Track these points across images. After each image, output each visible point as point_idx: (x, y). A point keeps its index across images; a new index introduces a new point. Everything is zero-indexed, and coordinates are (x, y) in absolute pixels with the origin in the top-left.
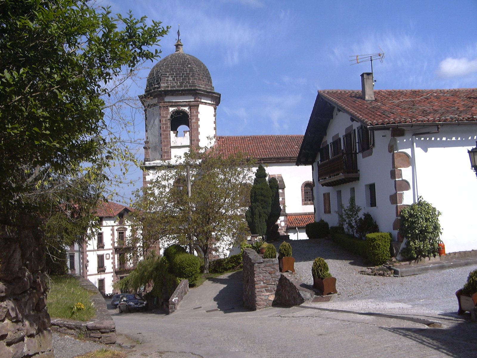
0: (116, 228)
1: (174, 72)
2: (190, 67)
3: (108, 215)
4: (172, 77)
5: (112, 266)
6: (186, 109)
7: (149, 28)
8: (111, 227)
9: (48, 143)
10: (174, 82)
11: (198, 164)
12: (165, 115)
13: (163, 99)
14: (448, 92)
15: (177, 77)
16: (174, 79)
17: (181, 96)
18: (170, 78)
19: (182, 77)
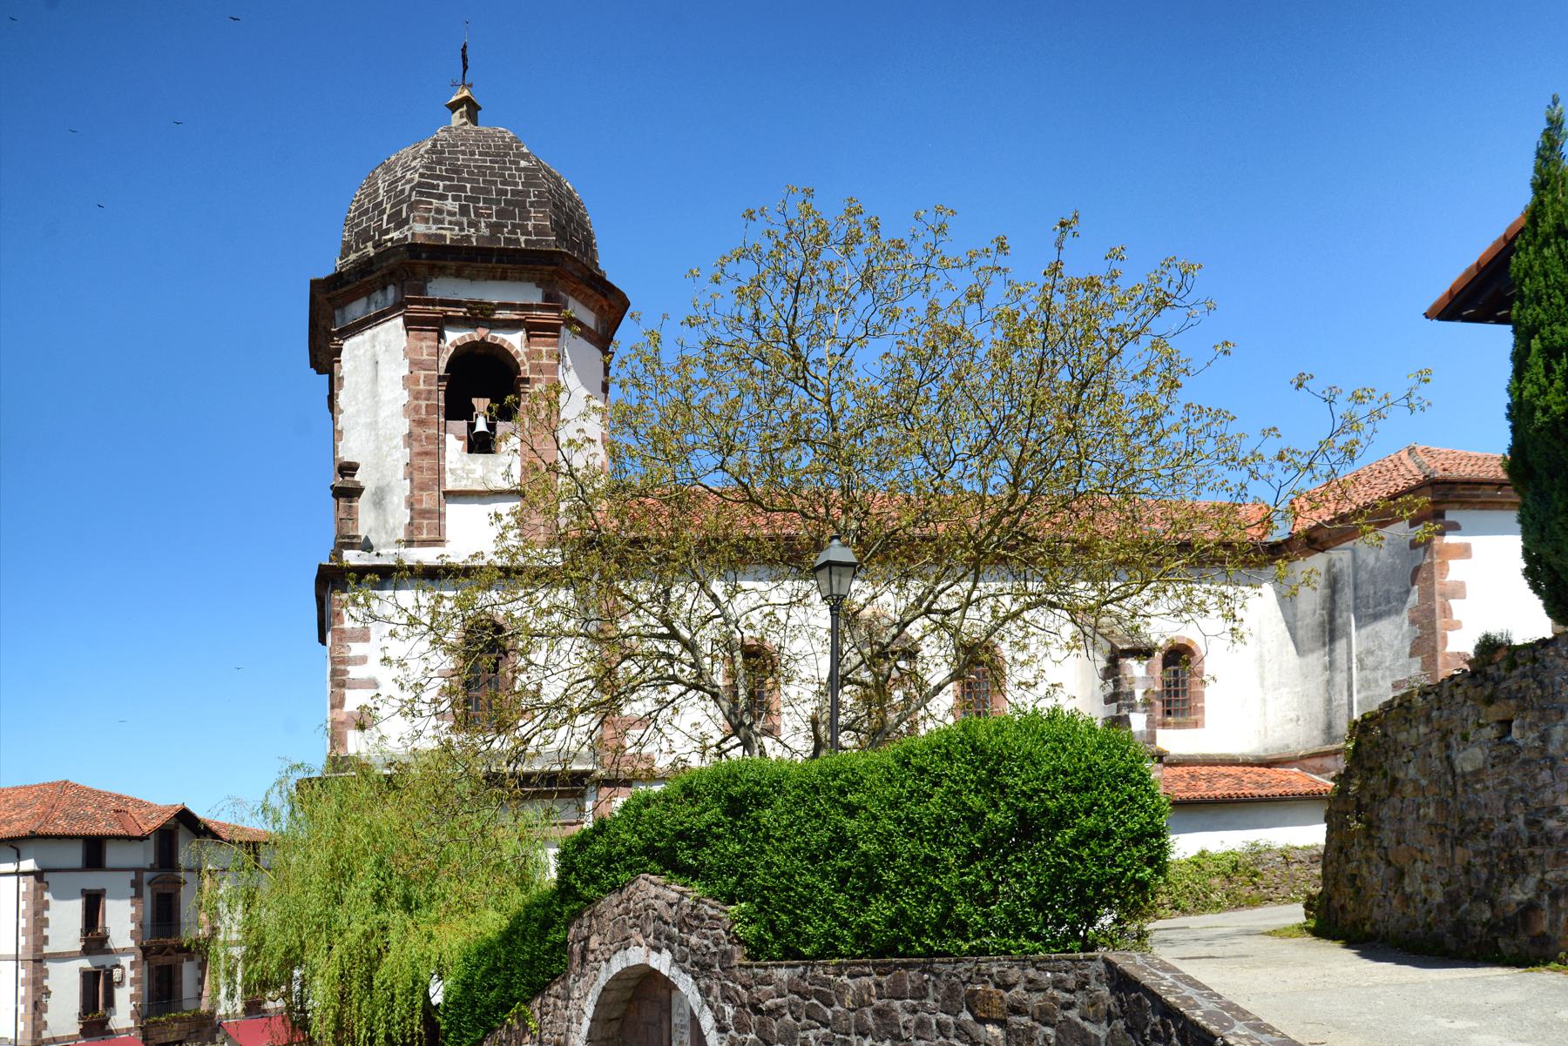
0: (147, 876)
1: (467, 180)
2: (524, 169)
3: (123, 832)
4: (455, 198)
5: (45, 1017)
6: (515, 341)
7: (725, 813)
8: (132, 875)
9: (240, 964)
10: (465, 220)
11: (571, 591)
12: (425, 357)
13: (422, 290)
14: (1213, 563)
15: (476, 200)
16: (464, 211)
17: (491, 283)
18: (450, 205)
19: (498, 202)
